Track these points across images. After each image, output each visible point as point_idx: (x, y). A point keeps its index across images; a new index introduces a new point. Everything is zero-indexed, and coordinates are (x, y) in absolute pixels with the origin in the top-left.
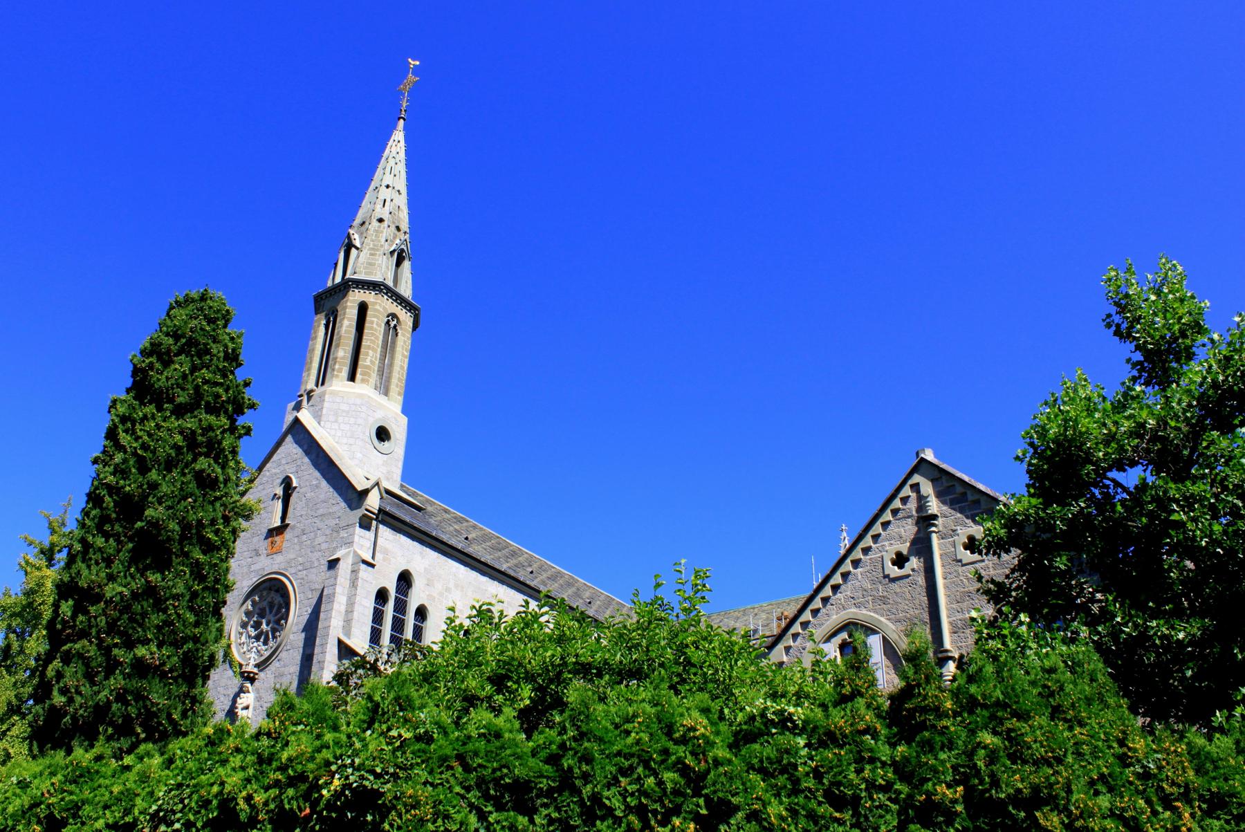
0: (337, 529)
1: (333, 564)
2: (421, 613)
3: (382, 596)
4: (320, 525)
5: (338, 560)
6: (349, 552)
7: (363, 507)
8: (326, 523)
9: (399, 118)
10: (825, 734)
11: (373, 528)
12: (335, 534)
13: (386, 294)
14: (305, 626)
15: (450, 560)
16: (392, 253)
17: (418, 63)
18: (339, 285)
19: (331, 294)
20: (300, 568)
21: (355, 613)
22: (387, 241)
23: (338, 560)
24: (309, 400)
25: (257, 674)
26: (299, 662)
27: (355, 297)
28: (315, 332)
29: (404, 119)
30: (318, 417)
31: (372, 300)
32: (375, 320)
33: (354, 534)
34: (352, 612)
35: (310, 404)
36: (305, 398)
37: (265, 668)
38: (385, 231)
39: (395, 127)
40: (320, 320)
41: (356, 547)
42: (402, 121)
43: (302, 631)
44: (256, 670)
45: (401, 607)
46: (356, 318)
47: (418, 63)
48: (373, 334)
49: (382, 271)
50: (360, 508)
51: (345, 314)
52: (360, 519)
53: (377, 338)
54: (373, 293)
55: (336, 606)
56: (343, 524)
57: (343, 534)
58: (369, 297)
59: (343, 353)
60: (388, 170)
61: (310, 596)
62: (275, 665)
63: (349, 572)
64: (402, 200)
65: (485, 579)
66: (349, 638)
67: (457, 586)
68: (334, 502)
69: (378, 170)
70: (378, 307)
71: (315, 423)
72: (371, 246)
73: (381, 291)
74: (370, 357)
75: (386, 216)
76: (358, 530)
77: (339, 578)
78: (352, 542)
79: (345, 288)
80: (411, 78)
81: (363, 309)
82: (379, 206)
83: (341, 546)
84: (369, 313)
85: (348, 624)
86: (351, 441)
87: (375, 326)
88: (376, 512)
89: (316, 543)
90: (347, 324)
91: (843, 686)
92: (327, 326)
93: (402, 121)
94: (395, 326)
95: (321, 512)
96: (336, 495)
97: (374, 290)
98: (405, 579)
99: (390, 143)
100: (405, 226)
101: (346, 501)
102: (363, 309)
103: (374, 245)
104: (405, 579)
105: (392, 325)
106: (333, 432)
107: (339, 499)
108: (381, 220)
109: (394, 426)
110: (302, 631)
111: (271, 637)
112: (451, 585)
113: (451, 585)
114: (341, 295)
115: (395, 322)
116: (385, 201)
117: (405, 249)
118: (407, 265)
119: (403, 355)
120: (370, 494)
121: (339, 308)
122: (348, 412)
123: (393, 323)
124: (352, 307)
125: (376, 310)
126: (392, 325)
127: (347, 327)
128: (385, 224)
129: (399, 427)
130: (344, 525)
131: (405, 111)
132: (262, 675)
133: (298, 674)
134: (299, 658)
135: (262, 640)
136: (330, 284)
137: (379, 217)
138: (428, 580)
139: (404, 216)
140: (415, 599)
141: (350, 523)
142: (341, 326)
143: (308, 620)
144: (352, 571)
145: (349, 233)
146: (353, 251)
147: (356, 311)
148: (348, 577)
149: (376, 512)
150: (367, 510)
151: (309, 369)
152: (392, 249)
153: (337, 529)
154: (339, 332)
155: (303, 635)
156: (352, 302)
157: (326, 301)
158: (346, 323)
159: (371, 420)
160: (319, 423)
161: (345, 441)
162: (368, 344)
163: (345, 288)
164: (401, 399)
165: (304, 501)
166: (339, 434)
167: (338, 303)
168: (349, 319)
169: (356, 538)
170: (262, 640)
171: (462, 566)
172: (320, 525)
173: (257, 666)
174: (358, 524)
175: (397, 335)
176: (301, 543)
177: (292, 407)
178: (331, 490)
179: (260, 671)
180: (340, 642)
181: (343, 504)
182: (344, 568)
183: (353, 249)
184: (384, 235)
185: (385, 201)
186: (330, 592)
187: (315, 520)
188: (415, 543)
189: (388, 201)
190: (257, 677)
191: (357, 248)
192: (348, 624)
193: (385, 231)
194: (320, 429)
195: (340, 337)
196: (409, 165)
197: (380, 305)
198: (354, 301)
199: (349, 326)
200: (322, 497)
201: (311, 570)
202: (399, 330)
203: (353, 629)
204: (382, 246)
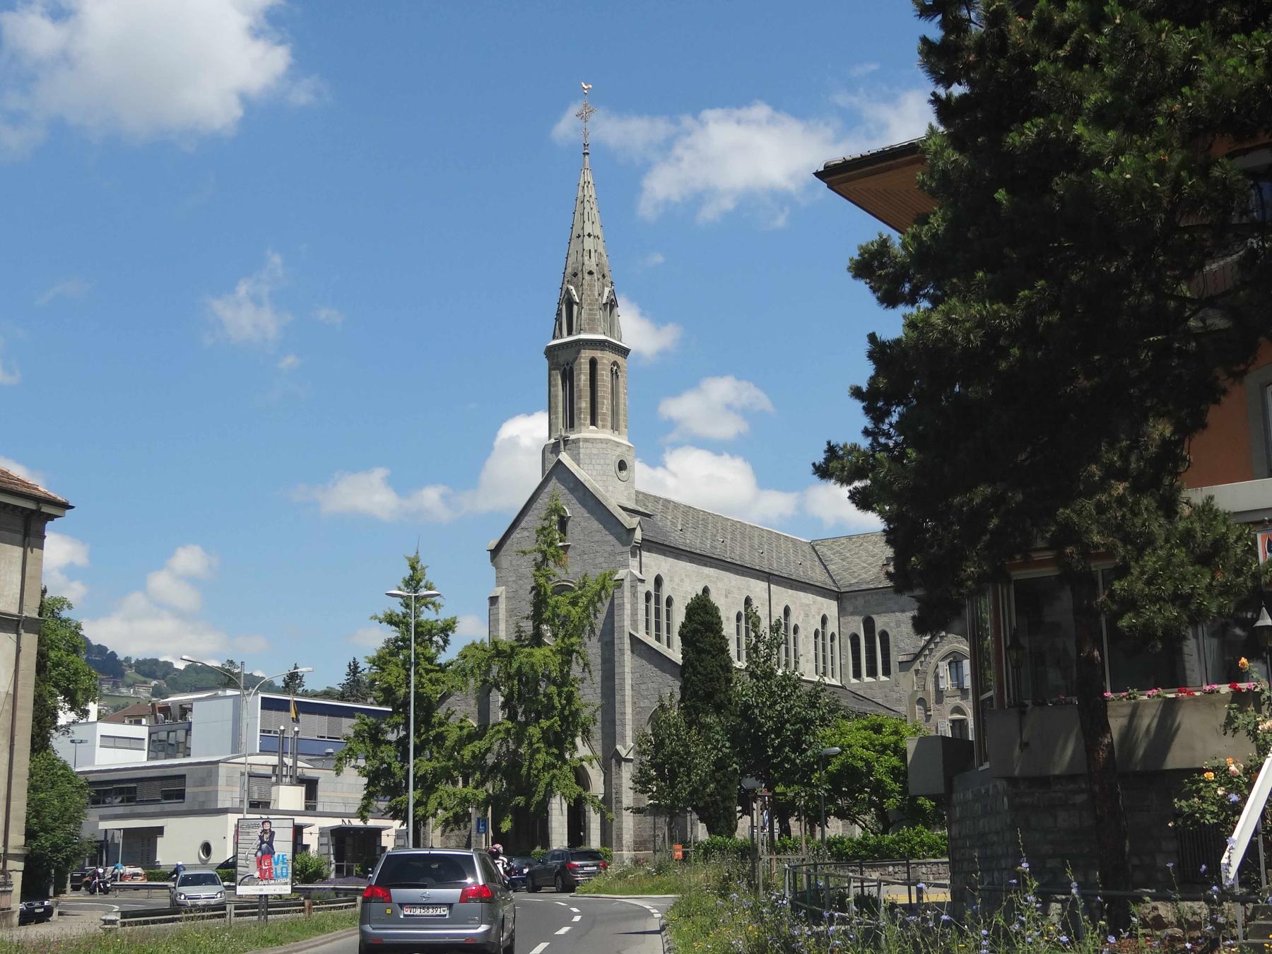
0: (613, 554)
2: (669, 601)
3: (648, 595)
8: (603, 548)
24: (565, 445)
27: (586, 355)
30: (577, 460)
34: (637, 614)
35: (567, 447)
38: (596, 284)
45: (658, 602)
53: (607, 388)
57: (619, 558)
58: (598, 354)
59: (584, 404)
71: (576, 467)
74: (604, 407)
75: (594, 269)
81: (593, 363)
84: (599, 367)
86: (604, 478)
90: (583, 379)
91: (1099, 32)
95: (596, 539)
98: (658, 581)
102: (593, 363)
106: (590, 472)
108: (591, 273)
112: (683, 577)
113: (683, 577)
120: (636, 531)
122: (598, 455)
124: (585, 363)
125: (604, 364)
138: (671, 577)
142: (580, 379)
144: (632, 586)
146: (575, 307)
153: (613, 554)
156: (585, 358)
158: (583, 377)
160: (579, 465)
161: (599, 478)
165: (579, 528)
166: (595, 473)
175: (617, 377)
180: (630, 634)
182: (627, 584)
189: (593, 251)
191: (577, 304)
194: (582, 472)
195: (581, 390)
198: (585, 358)
204: (597, 300)
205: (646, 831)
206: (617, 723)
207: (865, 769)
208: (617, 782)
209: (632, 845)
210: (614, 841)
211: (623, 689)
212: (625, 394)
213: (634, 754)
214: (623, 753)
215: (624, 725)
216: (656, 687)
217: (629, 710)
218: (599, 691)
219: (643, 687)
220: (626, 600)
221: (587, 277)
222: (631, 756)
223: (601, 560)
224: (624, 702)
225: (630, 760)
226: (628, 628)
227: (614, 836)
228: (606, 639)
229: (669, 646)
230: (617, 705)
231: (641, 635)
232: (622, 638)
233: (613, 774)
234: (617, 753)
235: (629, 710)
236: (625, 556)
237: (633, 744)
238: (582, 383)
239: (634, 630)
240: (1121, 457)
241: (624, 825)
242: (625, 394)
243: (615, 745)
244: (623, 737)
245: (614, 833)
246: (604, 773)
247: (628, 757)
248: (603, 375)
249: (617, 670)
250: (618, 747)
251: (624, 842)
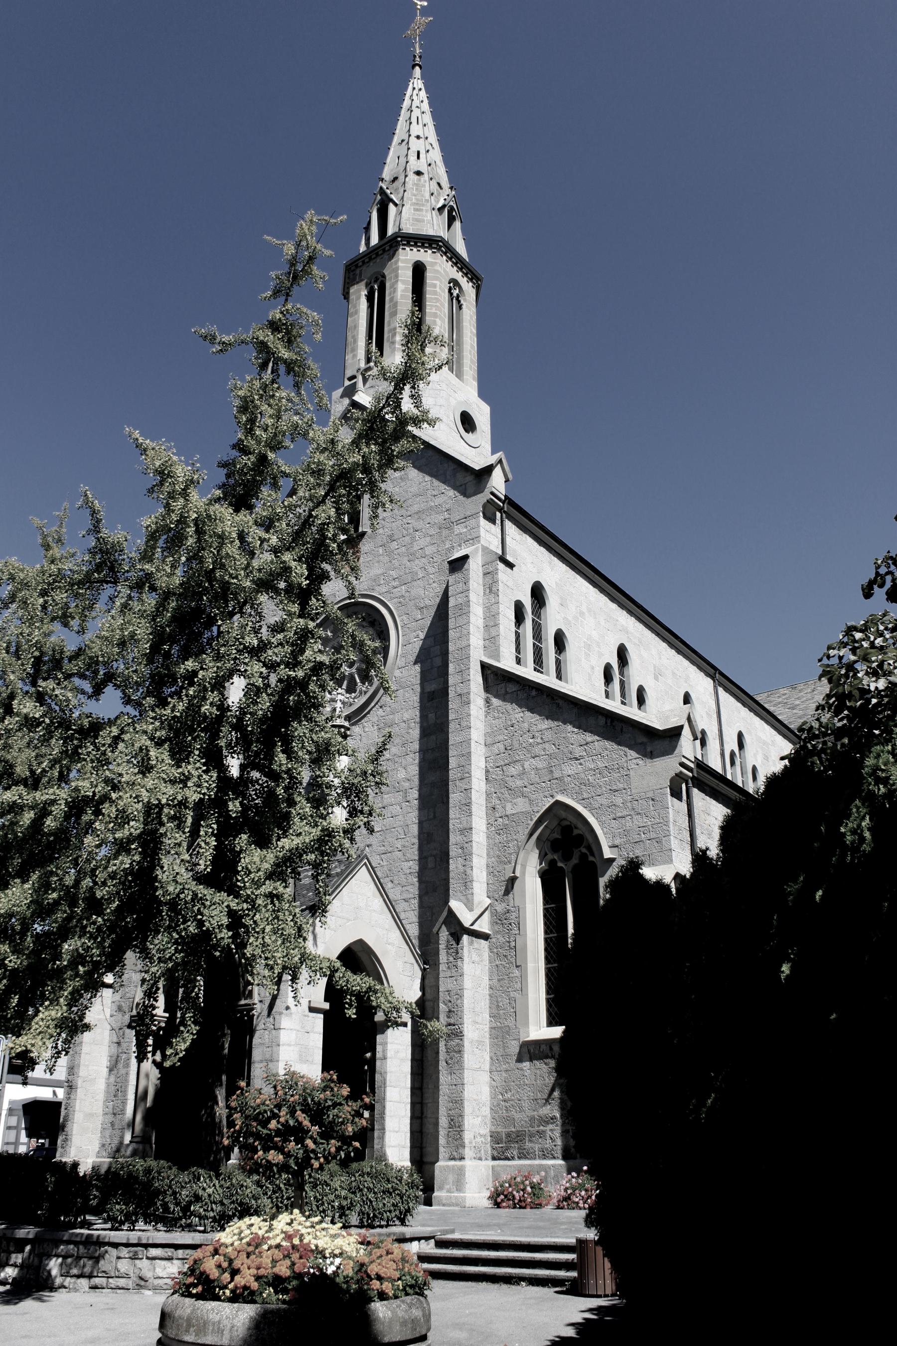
0: (448, 525)
1: (458, 564)
4: (419, 525)
5: (465, 558)
6: (477, 549)
7: (487, 491)
8: (428, 520)
9: (414, 66)
10: (242, 941)
11: (498, 522)
12: (445, 532)
13: (445, 253)
14: (418, 657)
15: (578, 577)
16: (441, 210)
17: (425, 4)
18: (377, 247)
19: (364, 263)
20: (395, 583)
21: (501, 627)
22: (432, 194)
23: (465, 558)
25: (349, 729)
26: (417, 705)
27: (407, 257)
28: (355, 306)
29: (420, 67)
31: (429, 259)
32: (437, 282)
33: (479, 526)
34: (496, 625)
35: (368, 385)
36: (360, 378)
37: (368, 713)
39: (410, 76)
40: (359, 291)
41: (483, 542)
42: (417, 68)
43: (415, 663)
44: (346, 724)
46: (411, 280)
47: (425, 4)
48: (437, 300)
49: (435, 226)
50: (482, 492)
51: (397, 276)
52: (484, 506)
53: (443, 306)
54: (430, 252)
55: (473, 619)
56: (456, 517)
57: (459, 529)
58: (426, 256)
60: (414, 120)
61: (419, 617)
62: (376, 715)
63: (481, 574)
64: (436, 155)
65: (614, 606)
66: (499, 661)
67: (589, 610)
68: (434, 493)
69: (400, 123)
70: (438, 268)
72: (414, 201)
73: (439, 249)
75: (423, 168)
76: (483, 522)
77: (471, 582)
78: (479, 537)
79: (391, 247)
80: (421, 21)
81: (419, 271)
82: (412, 158)
83: (460, 546)
85: (492, 641)
87: (438, 289)
88: (503, 498)
89: (416, 548)
92: (370, 298)
93: (417, 68)
94: (458, 296)
95: (416, 508)
96: (436, 483)
97: (430, 247)
99: (409, 92)
100: (445, 183)
101: (455, 488)
102: (419, 271)
103: (417, 200)
104: (538, 593)
105: (455, 294)
107: (443, 487)
108: (419, 173)
109: (478, 415)
110: (415, 663)
111: (358, 681)
113: (584, 609)
114: (386, 256)
115: (457, 291)
116: (418, 153)
117: (455, 206)
118: (457, 224)
119: (471, 332)
120: (683, 733)
121: (386, 272)
123: (456, 292)
124: (405, 268)
126: (455, 294)
127: (403, 291)
128: (426, 177)
129: (482, 414)
130: (458, 518)
131: (420, 57)
132: (356, 729)
133: (418, 720)
134: (417, 698)
135: (344, 686)
136: (363, 248)
137: (416, 170)
138: (562, 598)
139: (441, 172)
140: (553, 621)
141: (469, 513)
142: (395, 290)
143: (422, 649)
145: (381, 188)
146: (392, 209)
147: (410, 273)
148: (481, 581)
149: (503, 498)
150: (336, 603)
151: (354, 350)
152: (440, 205)
153: (448, 525)
154: (392, 299)
155: (418, 668)
157: (364, 268)
159: (453, 402)
162: (434, 310)
163: (391, 247)
164: (475, 384)
167: (384, 266)
168: (404, 282)
169: (482, 533)
170: (344, 686)
171: (591, 587)
172: (419, 525)
173: (348, 718)
174: (481, 514)
175: (460, 307)
176: (390, 553)
177: (340, 395)
178: (428, 478)
179: (352, 725)
181: (451, 493)
182: (475, 567)
183: (391, 206)
184: (427, 188)
185: (418, 153)
186: (460, 601)
187: (409, 520)
188: (542, 549)
190: (348, 733)
192: (492, 641)
193: (427, 184)
196: (435, 115)
197: (441, 266)
198: (405, 261)
199: (405, 290)
200: (414, 489)
201: (415, 583)
202: (462, 302)
203: (501, 649)
204: (427, 201)
205: (521, 1110)
206: (451, 854)
207: (390, 427)
208: (450, 986)
209: (487, 1149)
210: (442, 1133)
211: (466, 776)
212: (531, 820)
213: (493, 923)
214: (466, 918)
215: (467, 856)
216: (540, 766)
217: (479, 822)
218: (415, 794)
219: (512, 770)
220: (473, 597)
221: (412, 177)
222: (483, 926)
223: (422, 542)
224: (468, 804)
225: (485, 937)
226: (478, 654)
227: (443, 1121)
228: (432, 687)
229: (559, 677)
230: (453, 813)
231: (507, 663)
232: (463, 672)
233: (442, 967)
234: (452, 920)
235: (479, 822)
236: (472, 522)
237: (488, 901)
238: (399, 293)
239: (490, 657)
240: (338, 546)
241: (469, 1093)
242: (531, 820)
243: (447, 901)
244: (467, 883)
245: (442, 1111)
246: (424, 971)
247: (475, 927)
248: (435, 286)
249: (453, 739)
250: (455, 905)
251: (468, 1136)
